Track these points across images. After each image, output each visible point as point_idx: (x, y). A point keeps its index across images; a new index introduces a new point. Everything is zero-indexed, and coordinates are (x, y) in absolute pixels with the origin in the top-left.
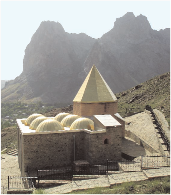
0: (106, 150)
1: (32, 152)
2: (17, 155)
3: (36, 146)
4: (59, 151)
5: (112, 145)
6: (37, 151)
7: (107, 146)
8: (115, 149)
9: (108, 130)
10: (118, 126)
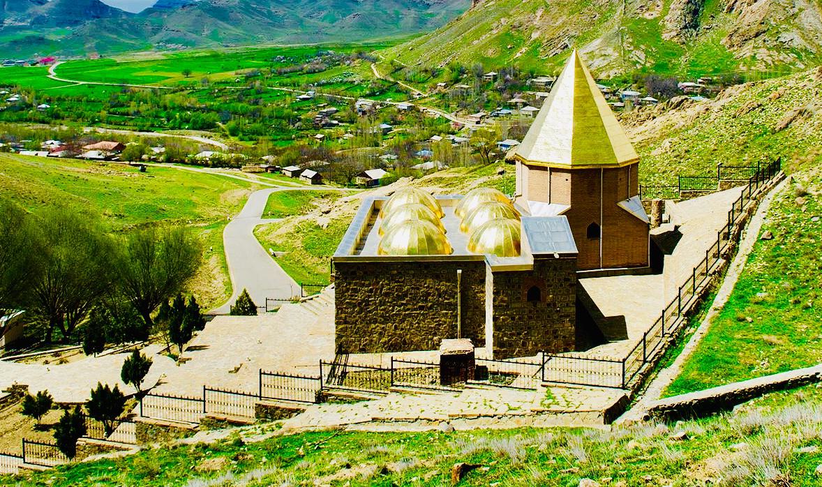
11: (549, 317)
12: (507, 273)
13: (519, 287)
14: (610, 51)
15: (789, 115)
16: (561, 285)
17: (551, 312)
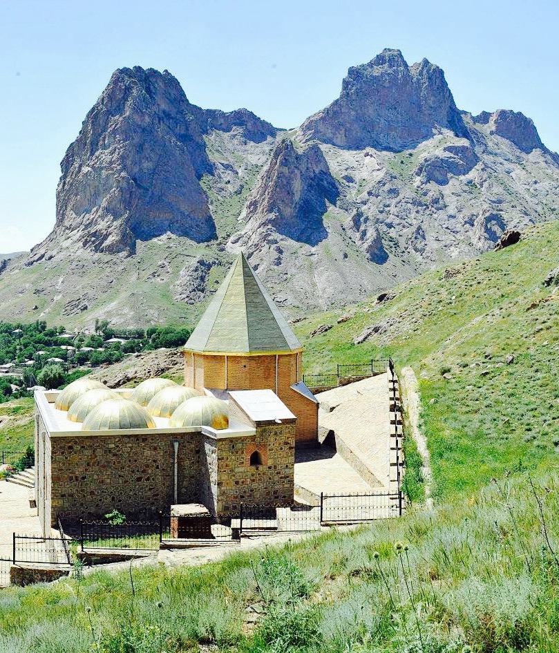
0: (253, 481)
1: (71, 479)
2: (34, 484)
3: (82, 465)
4: (139, 479)
5: (270, 468)
6: (84, 478)
7: (257, 469)
8: (276, 478)
9: (259, 430)
10: (285, 422)
11: (270, 479)
12: (64, 439)
13: (243, 452)
14: (126, 311)
15: (365, 332)
16: (281, 449)
17: (271, 474)
